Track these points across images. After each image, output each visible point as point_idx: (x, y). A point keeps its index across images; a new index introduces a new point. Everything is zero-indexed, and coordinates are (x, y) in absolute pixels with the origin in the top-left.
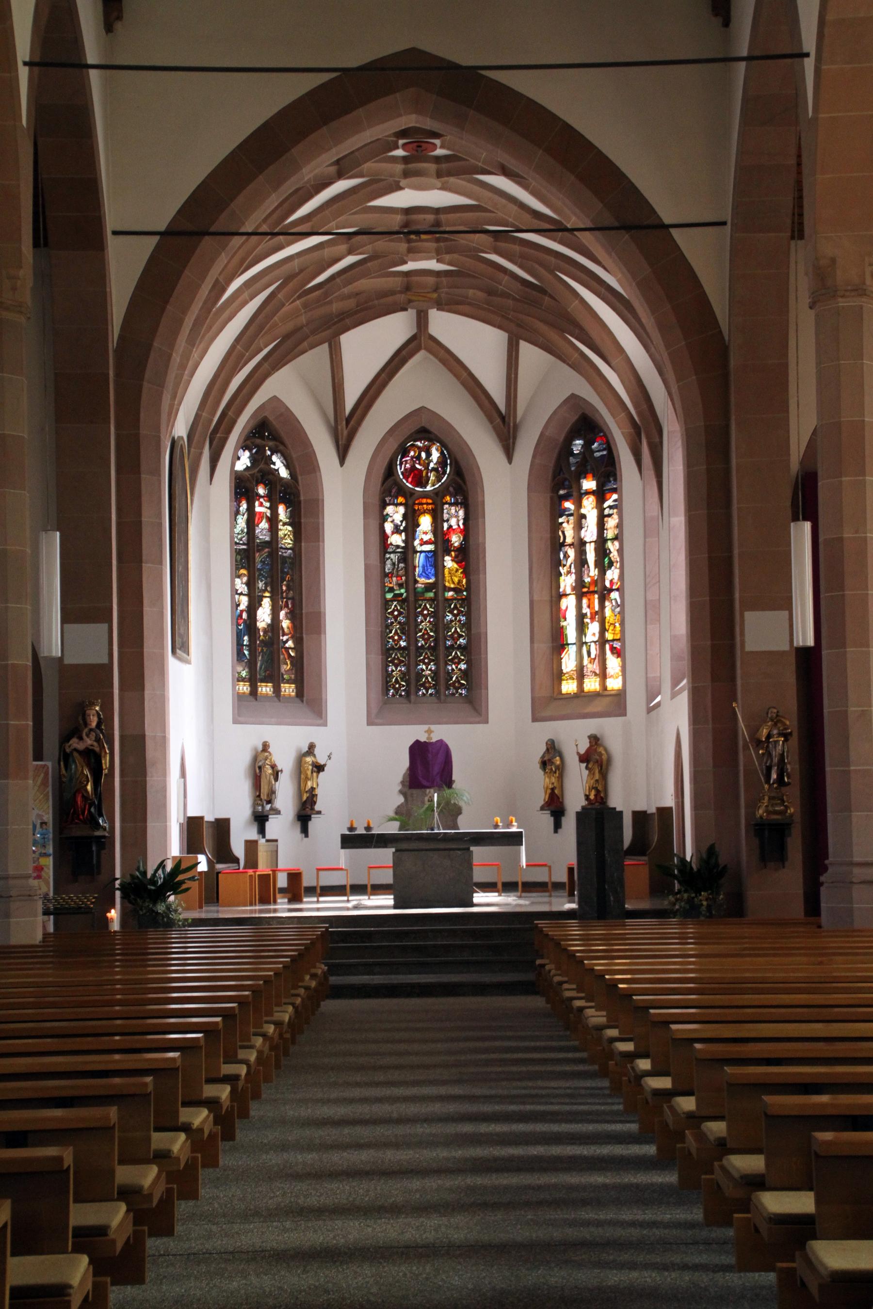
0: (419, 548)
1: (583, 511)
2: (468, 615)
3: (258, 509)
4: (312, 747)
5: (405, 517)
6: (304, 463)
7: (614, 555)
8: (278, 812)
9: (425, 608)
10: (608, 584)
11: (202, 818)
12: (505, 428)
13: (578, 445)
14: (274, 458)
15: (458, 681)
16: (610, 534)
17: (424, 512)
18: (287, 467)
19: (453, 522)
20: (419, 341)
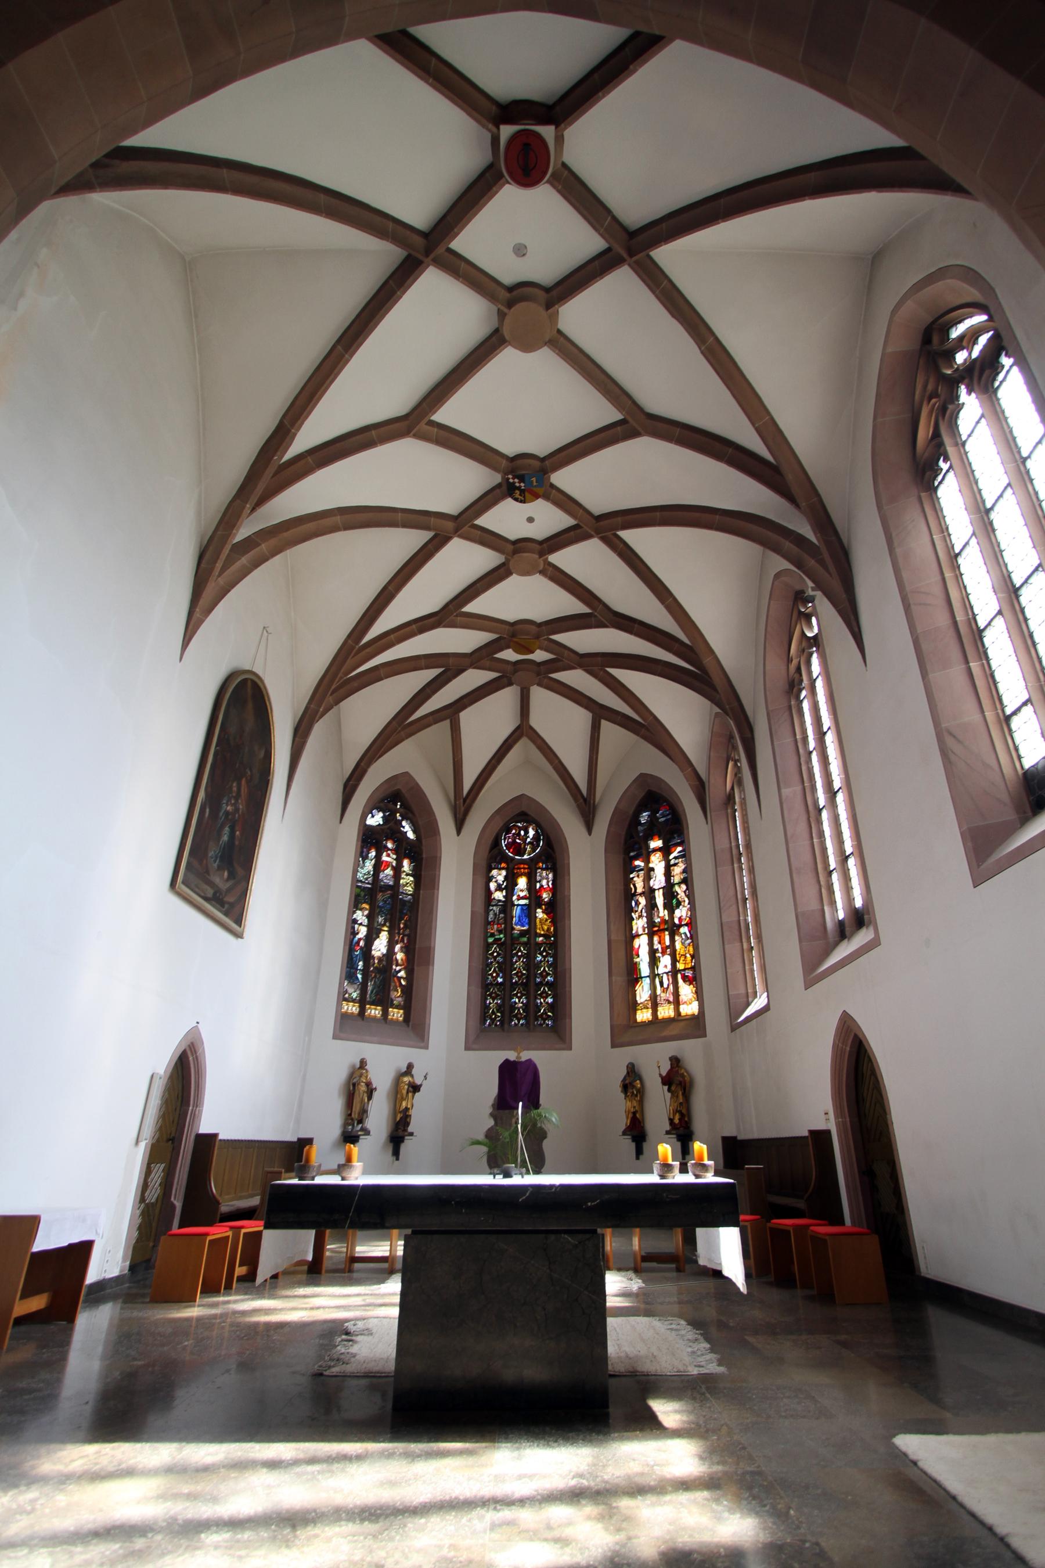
0: (516, 903)
1: (651, 865)
2: (555, 956)
3: (385, 858)
4: (410, 1066)
5: (506, 878)
6: (427, 828)
7: (682, 896)
8: (367, 1132)
9: (520, 950)
10: (676, 921)
11: (215, 1135)
12: (586, 808)
13: (644, 817)
14: (404, 823)
15: (545, 1012)
16: (676, 879)
17: (521, 875)
18: (414, 832)
19: (544, 882)
20: (523, 731)
